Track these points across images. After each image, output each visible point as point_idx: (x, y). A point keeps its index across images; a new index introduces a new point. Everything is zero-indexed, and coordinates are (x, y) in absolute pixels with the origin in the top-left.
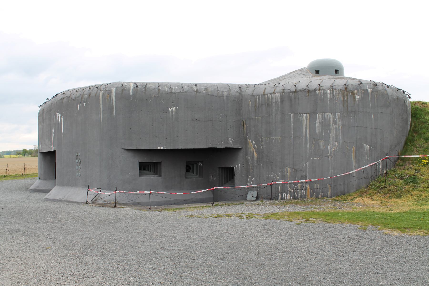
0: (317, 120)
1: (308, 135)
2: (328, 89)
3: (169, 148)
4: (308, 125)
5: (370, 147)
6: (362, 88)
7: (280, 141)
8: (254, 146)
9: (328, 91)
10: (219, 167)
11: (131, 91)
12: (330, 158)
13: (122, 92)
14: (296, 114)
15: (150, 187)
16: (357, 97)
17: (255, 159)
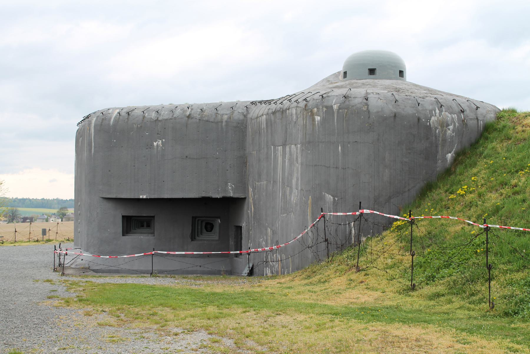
3: (153, 197)
5: (334, 199)
6: (325, 104)
11: (112, 120)
13: (102, 122)
14: (275, 146)
15: (135, 250)
16: (316, 119)
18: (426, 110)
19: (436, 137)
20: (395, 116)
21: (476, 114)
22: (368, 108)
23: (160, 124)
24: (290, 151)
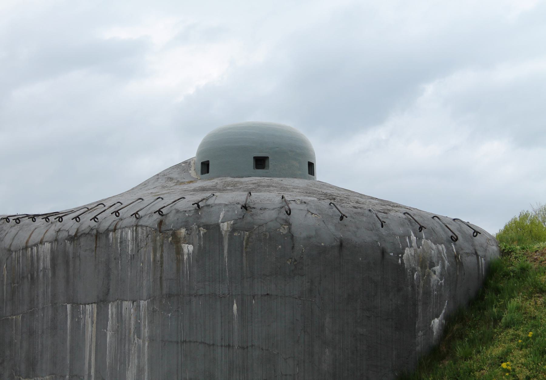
0: (110, 323)
1: (93, 371)
2: (129, 227)
6: (203, 220)
14: (76, 304)
16: (185, 250)
18: (395, 235)
19: (413, 287)
20: (341, 245)
21: (473, 245)
22: (290, 229)
24: (120, 316)
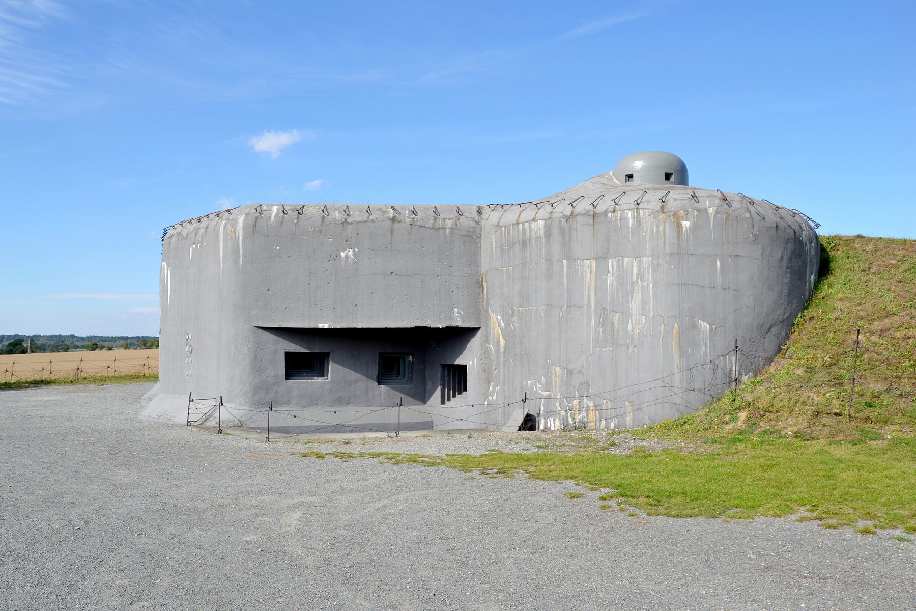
1: (593, 303)
4: (593, 283)
5: (711, 327)
7: (543, 315)
8: (499, 325)
9: (630, 215)
10: (444, 366)
12: (631, 349)
17: (502, 350)
23: (350, 227)
